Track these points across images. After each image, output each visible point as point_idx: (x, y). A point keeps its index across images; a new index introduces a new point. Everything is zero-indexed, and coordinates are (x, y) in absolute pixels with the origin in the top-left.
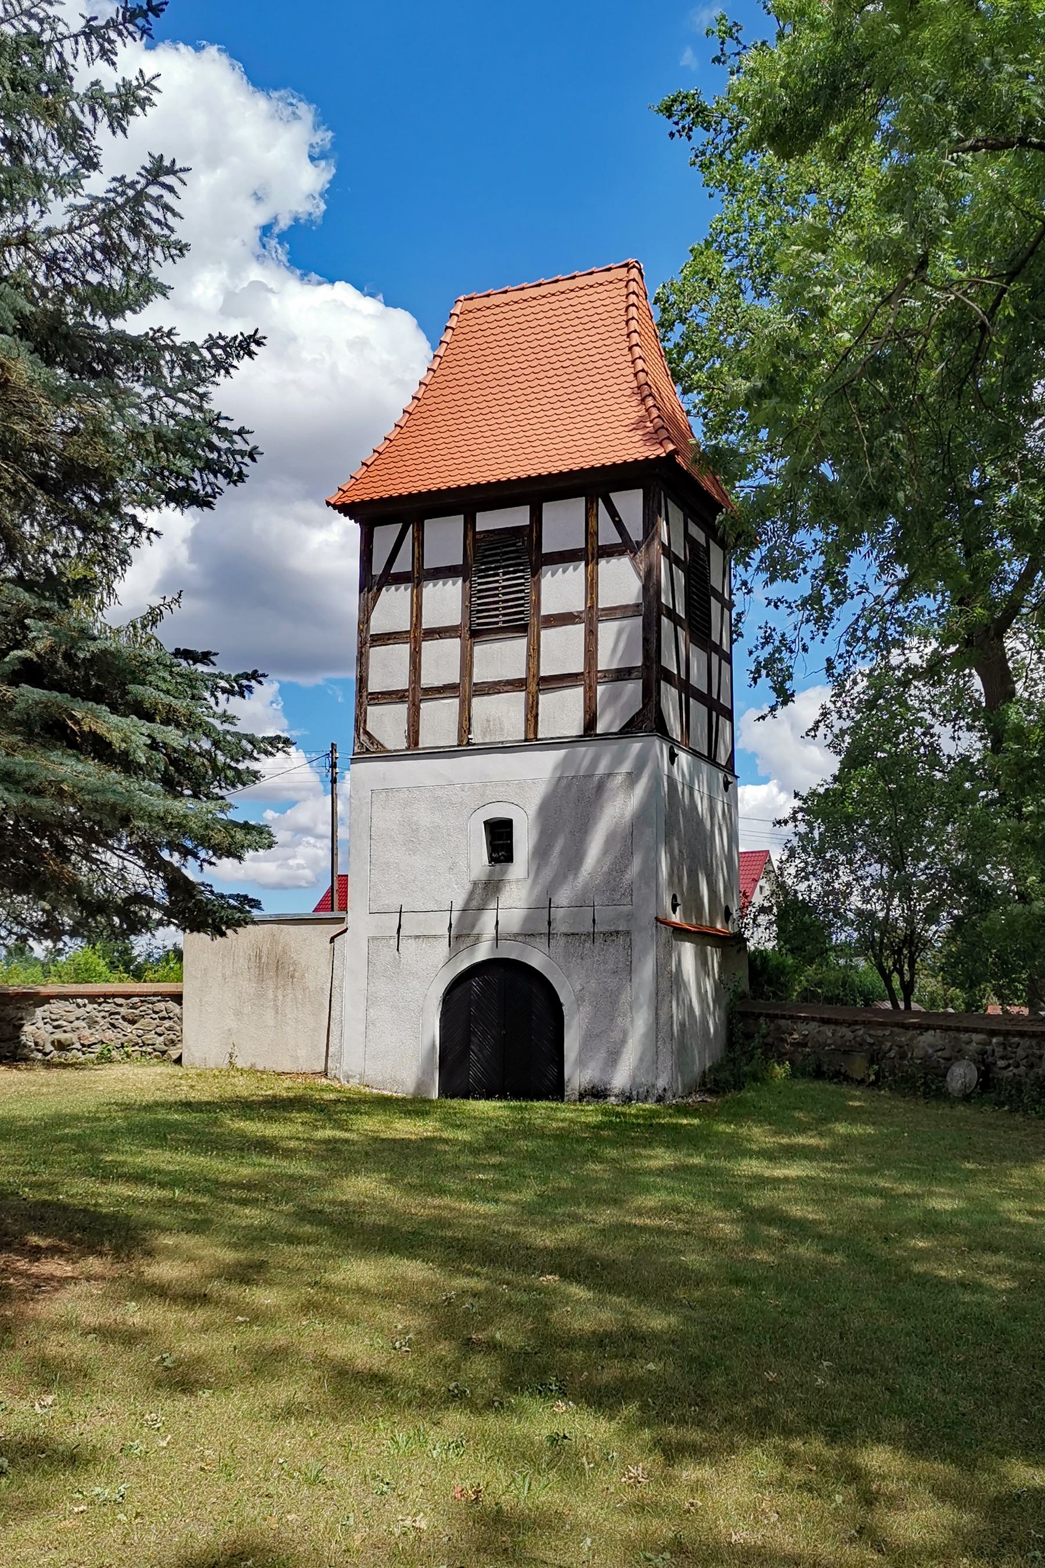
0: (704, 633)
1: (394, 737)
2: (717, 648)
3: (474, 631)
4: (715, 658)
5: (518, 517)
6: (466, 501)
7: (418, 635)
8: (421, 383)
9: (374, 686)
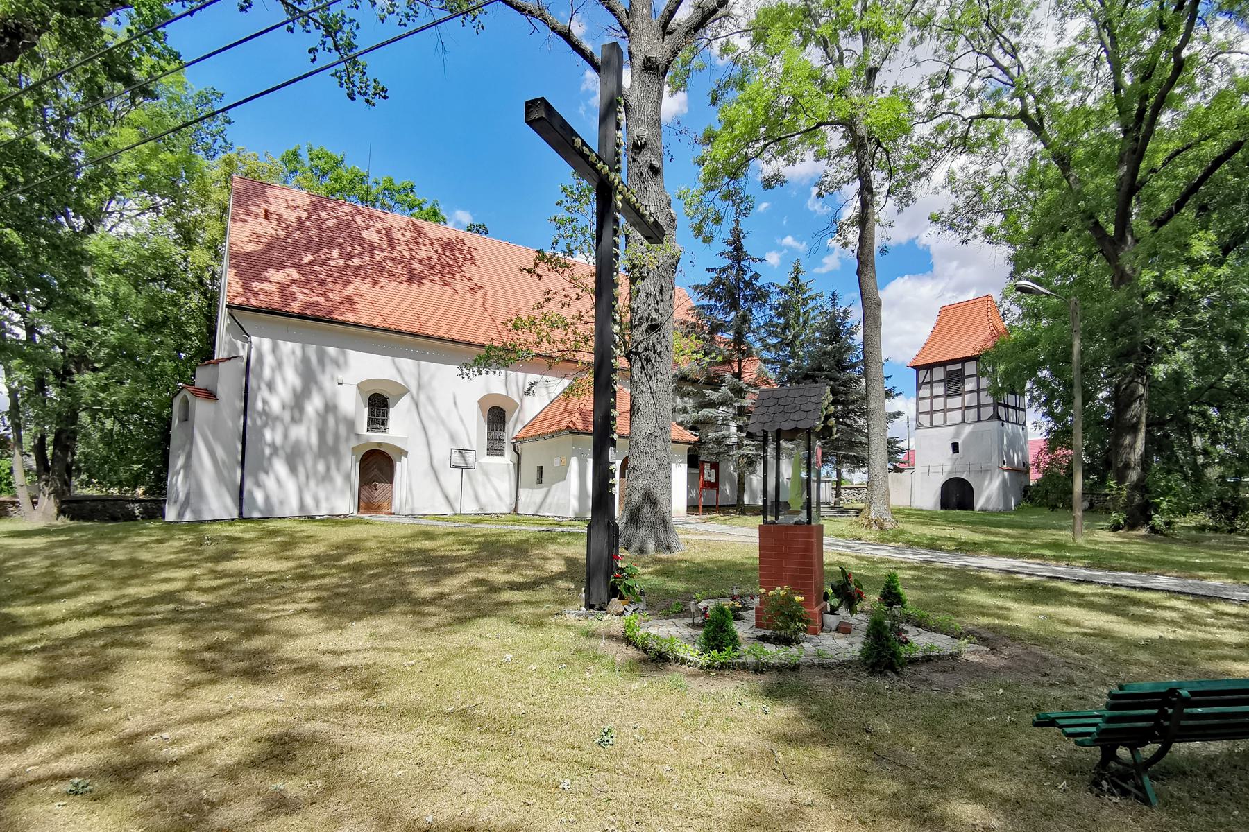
1: (927, 424)
5: (958, 366)
6: (944, 364)
7: (932, 397)
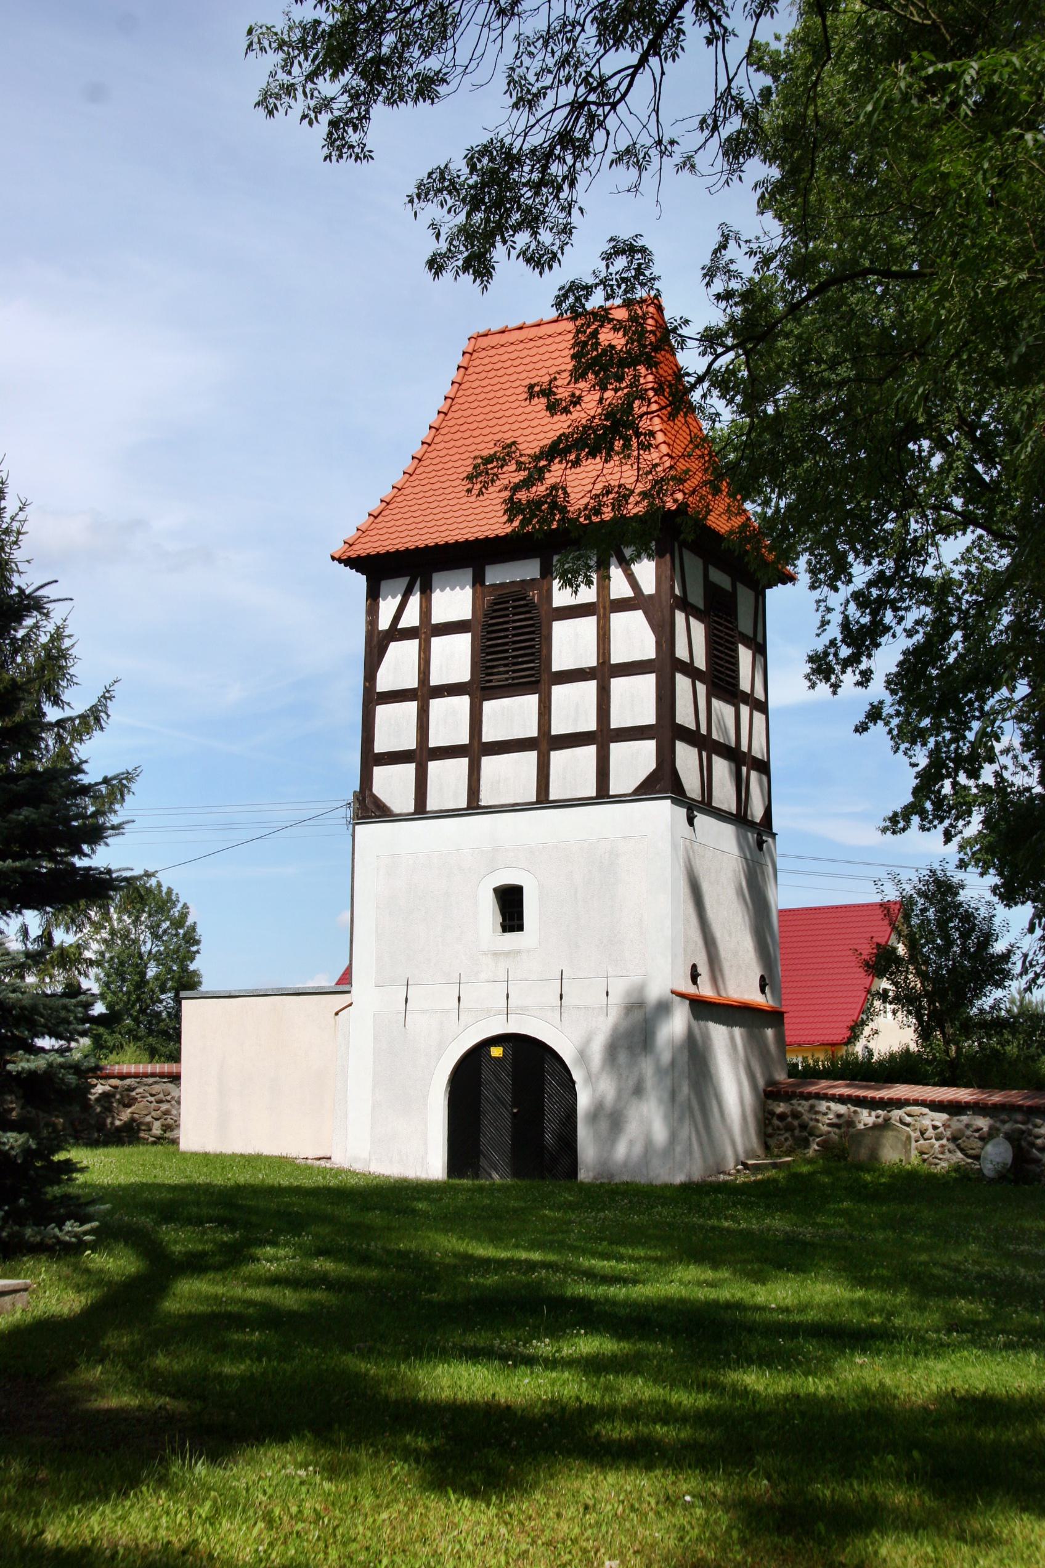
0: (728, 683)
2: (748, 699)
3: (483, 686)
4: (745, 710)
7: (424, 693)
8: (431, 427)
9: (379, 747)
